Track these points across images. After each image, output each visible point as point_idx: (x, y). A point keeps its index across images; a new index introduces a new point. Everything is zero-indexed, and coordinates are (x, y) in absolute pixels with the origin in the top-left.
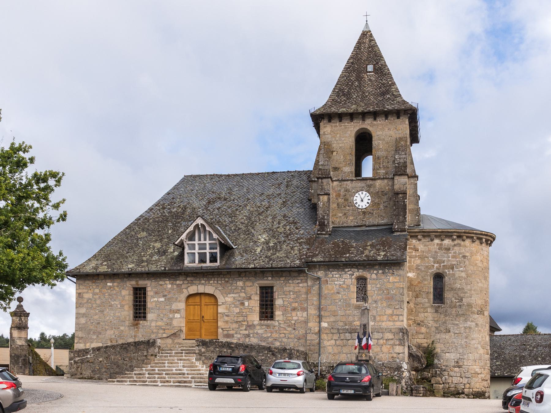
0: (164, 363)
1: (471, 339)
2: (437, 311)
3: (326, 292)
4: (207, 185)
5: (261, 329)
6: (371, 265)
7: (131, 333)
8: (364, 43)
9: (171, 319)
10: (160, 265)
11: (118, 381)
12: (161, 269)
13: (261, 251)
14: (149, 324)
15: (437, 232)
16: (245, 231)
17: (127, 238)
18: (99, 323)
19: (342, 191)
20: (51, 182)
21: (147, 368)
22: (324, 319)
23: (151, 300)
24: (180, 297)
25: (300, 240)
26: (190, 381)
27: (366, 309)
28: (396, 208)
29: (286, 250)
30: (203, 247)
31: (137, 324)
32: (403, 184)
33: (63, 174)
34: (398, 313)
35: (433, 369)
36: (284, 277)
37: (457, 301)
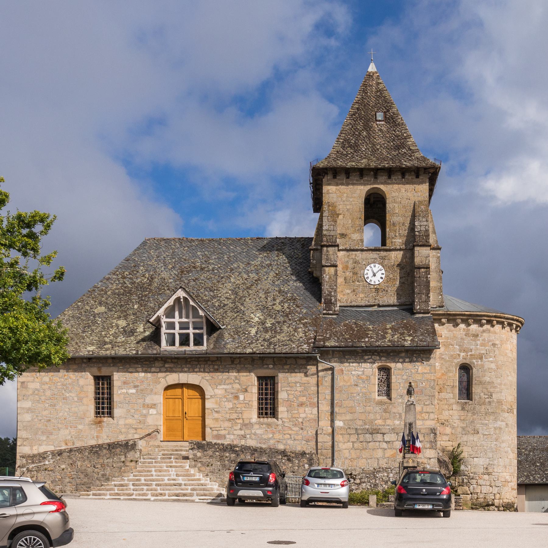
0: (151, 471)
1: (501, 442)
2: (464, 408)
3: (341, 384)
4: (176, 250)
5: (260, 428)
6: (396, 352)
7: (92, 432)
8: (370, 86)
9: (145, 416)
10: (129, 347)
11: (94, 495)
12: (132, 353)
13: (256, 332)
14: (115, 421)
15: (464, 315)
16: (232, 308)
17: (81, 314)
18: (50, 420)
19: (350, 263)
20: (38, 228)
21: (128, 477)
22: (338, 417)
23: (118, 392)
24: (156, 388)
25: (303, 320)
26: (190, 493)
27: (412, 404)
28: (418, 285)
29: (288, 332)
30: (184, 326)
31: (100, 422)
32: (425, 256)
33: (55, 217)
34: (428, 410)
35: (459, 476)
36: (288, 365)
37: (486, 396)
